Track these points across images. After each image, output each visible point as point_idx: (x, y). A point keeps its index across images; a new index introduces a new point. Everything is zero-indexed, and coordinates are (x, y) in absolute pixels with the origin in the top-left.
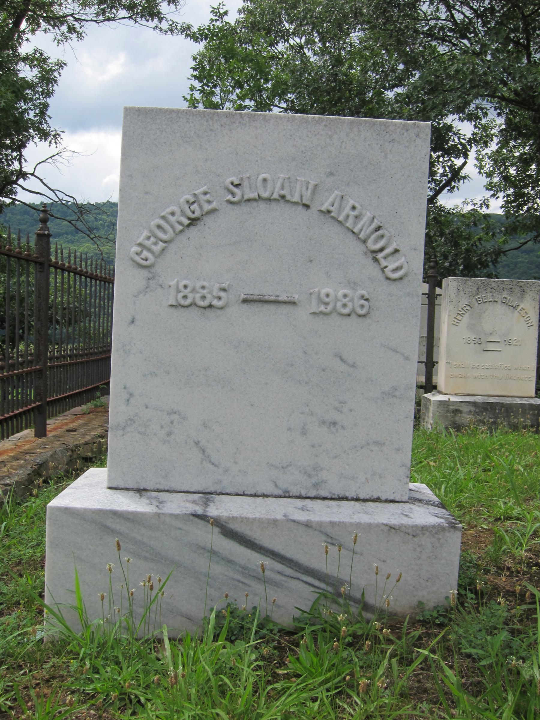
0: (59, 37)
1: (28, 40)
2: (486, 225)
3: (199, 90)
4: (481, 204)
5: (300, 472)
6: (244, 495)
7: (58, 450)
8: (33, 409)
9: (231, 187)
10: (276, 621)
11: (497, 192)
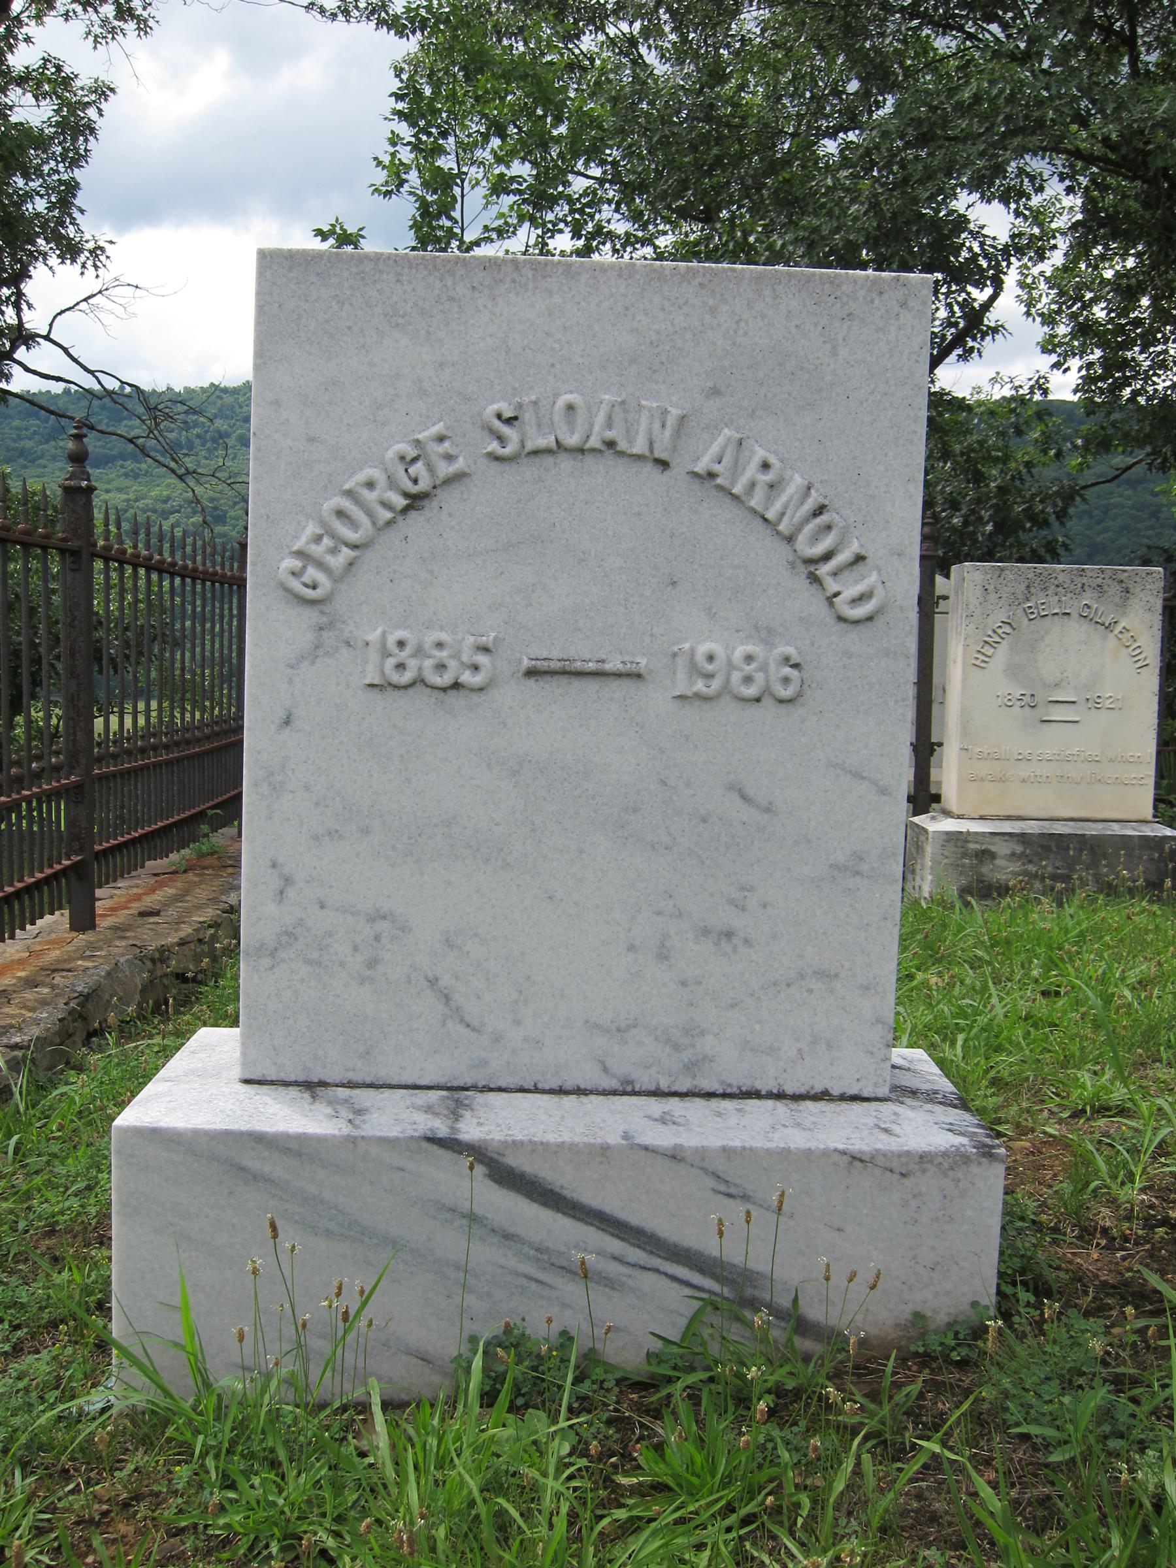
0: (97, 30)
1: (28, 40)
2: (1043, 433)
3: (409, 143)
4: (1032, 388)
5: (656, 1039)
6: (536, 1090)
7: (122, 960)
8: (65, 871)
9: (497, 424)
10: (612, 1362)
11: (1065, 356)
